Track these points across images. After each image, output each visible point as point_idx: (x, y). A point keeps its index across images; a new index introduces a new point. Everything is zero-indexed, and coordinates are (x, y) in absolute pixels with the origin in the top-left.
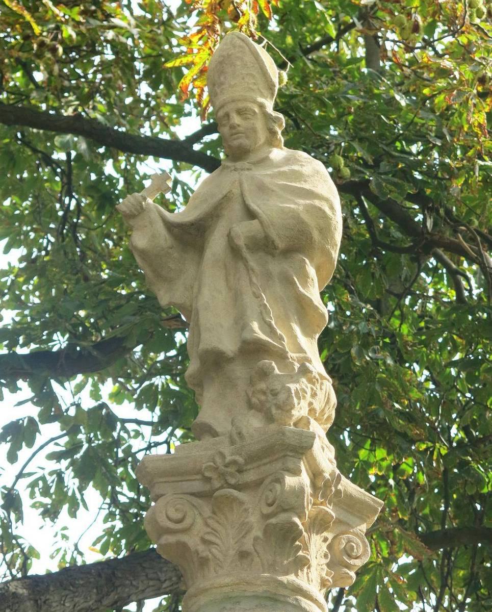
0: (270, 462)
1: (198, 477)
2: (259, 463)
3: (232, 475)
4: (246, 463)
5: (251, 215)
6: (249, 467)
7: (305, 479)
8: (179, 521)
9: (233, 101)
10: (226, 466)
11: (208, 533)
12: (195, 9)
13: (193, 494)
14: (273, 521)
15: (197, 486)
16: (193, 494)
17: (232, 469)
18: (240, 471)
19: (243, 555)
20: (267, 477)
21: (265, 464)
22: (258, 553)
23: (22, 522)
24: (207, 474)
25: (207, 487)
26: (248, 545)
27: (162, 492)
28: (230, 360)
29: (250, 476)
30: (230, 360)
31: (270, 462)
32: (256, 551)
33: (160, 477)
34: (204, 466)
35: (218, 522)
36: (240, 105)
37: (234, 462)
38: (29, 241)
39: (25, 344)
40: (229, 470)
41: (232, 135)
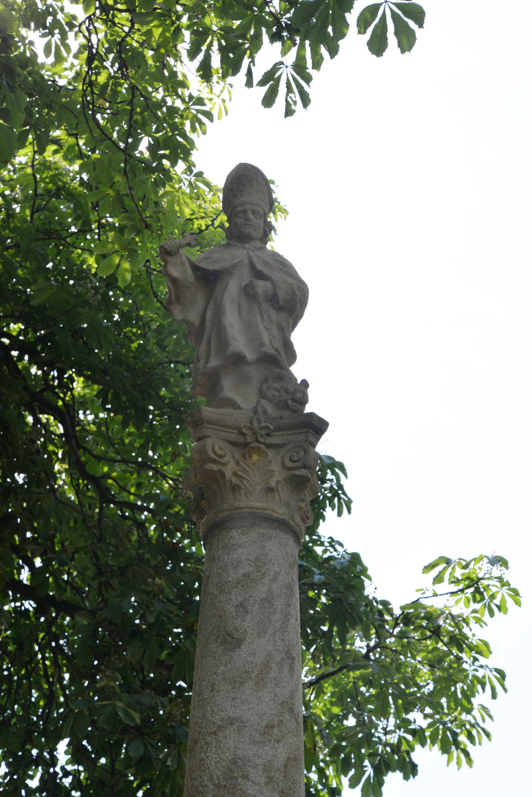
0: (293, 434)
1: (235, 431)
2: (284, 433)
3: (262, 436)
4: (275, 430)
6: (274, 434)
8: (221, 457)
9: (251, 203)
10: (260, 429)
11: (240, 471)
12: (195, 183)
13: (229, 442)
14: (297, 472)
15: (234, 436)
16: (229, 442)
17: (263, 432)
18: (268, 435)
19: (270, 490)
20: (289, 443)
21: (288, 435)
22: (278, 492)
23: (275, 232)
24: (244, 431)
25: (241, 439)
26: (273, 484)
27: (208, 434)
28: (248, 363)
29: (276, 440)
30: (248, 363)
31: (293, 434)
32: (277, 490)
33: (208, 424)
34: (242, 425)
35: (247, 465)
36: (254, 207)
37: (267, 428)
38: (50, 762)
39: (103, 118)
40: (261, 432)
41: (246, 225)
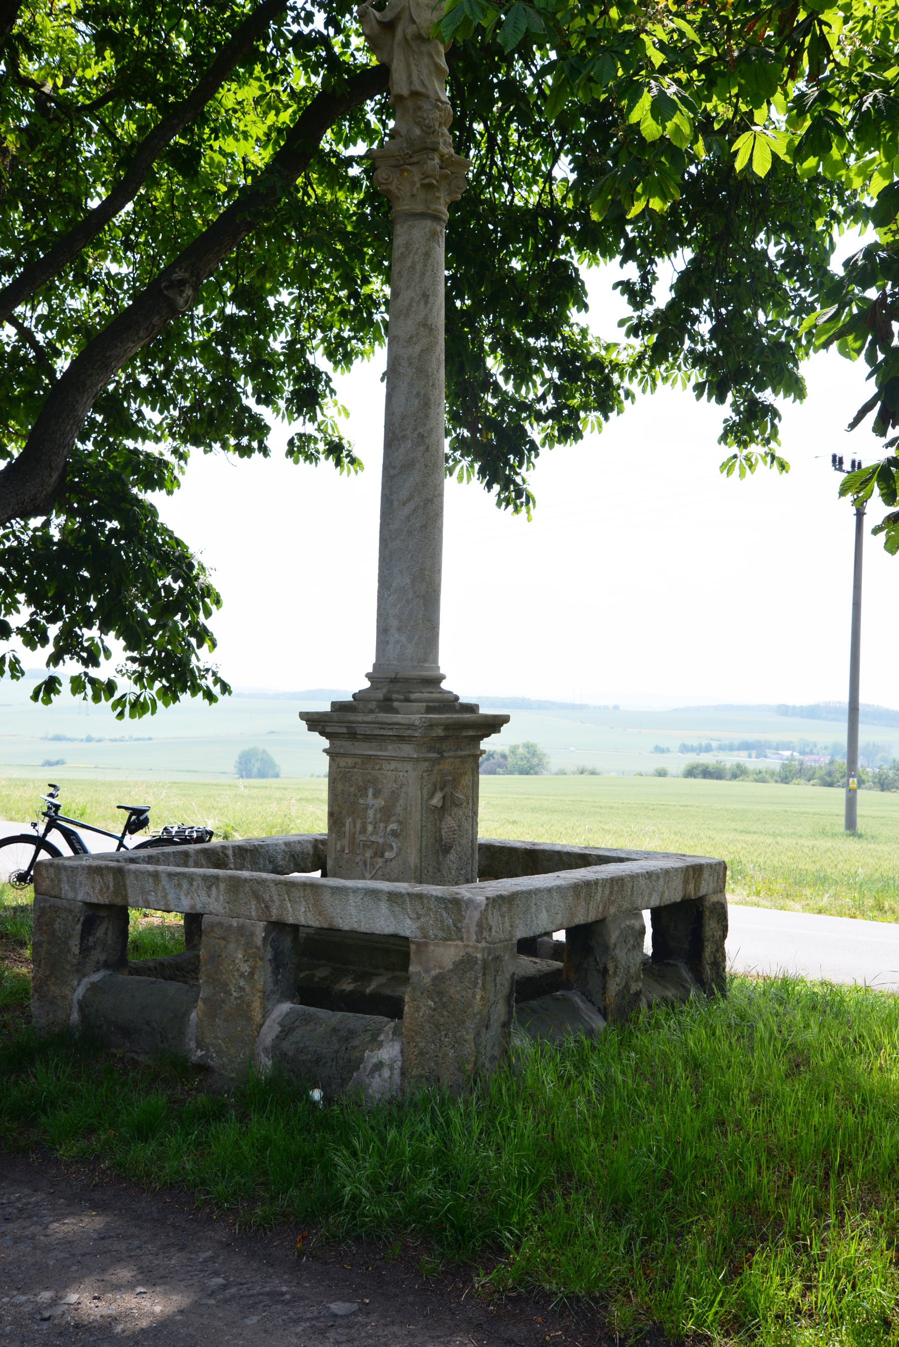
5: (413, 21)
7: (437, 161)
29: (415, 160)
